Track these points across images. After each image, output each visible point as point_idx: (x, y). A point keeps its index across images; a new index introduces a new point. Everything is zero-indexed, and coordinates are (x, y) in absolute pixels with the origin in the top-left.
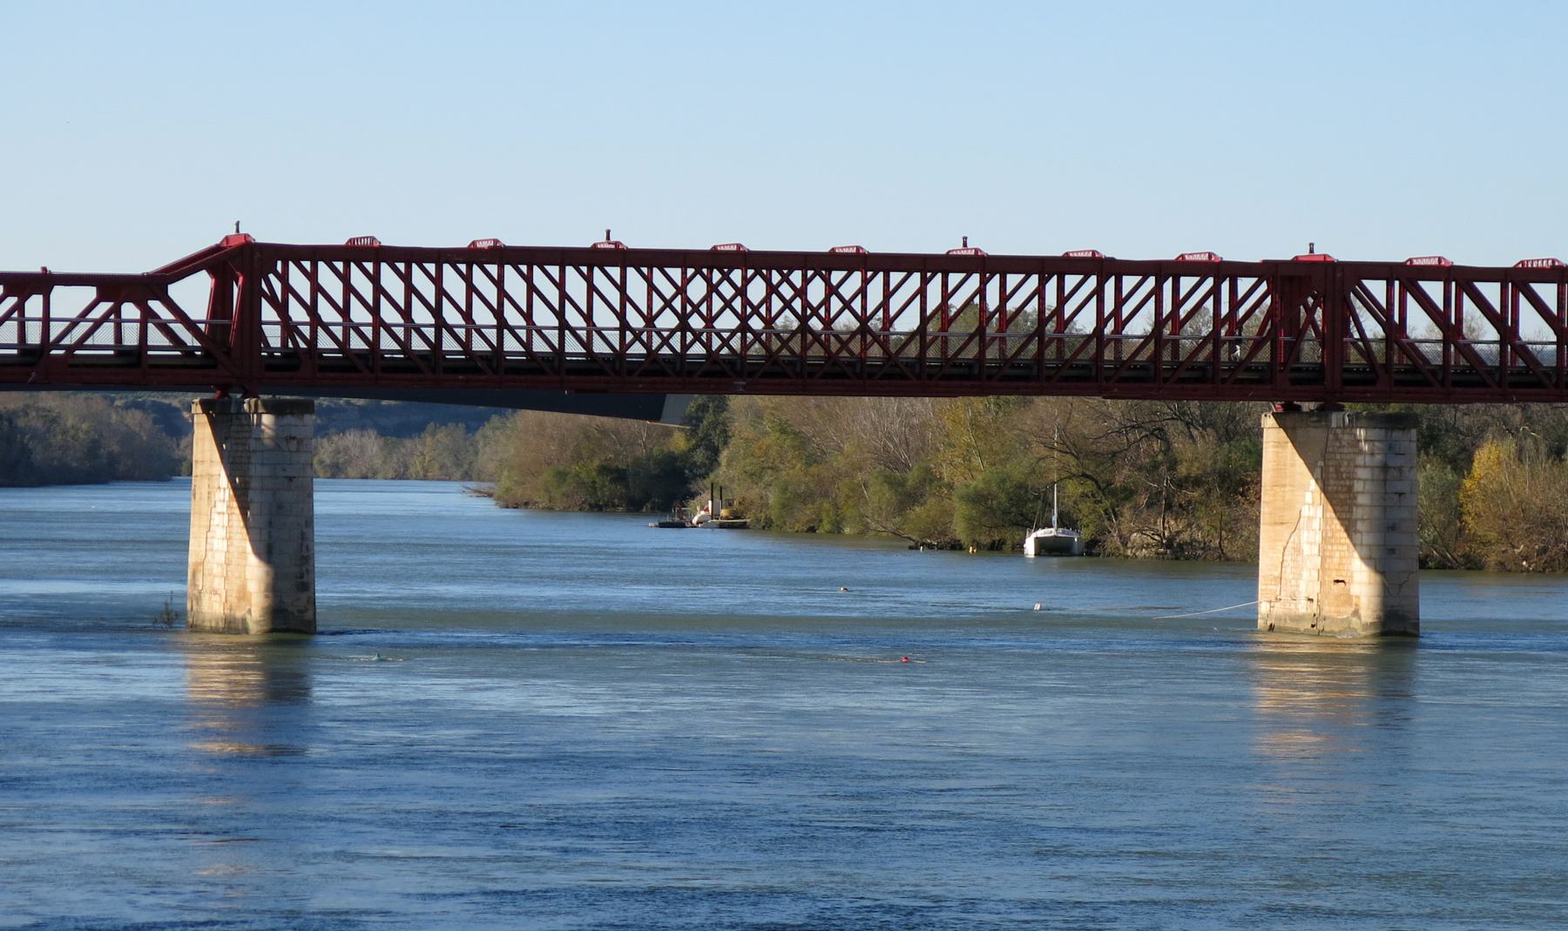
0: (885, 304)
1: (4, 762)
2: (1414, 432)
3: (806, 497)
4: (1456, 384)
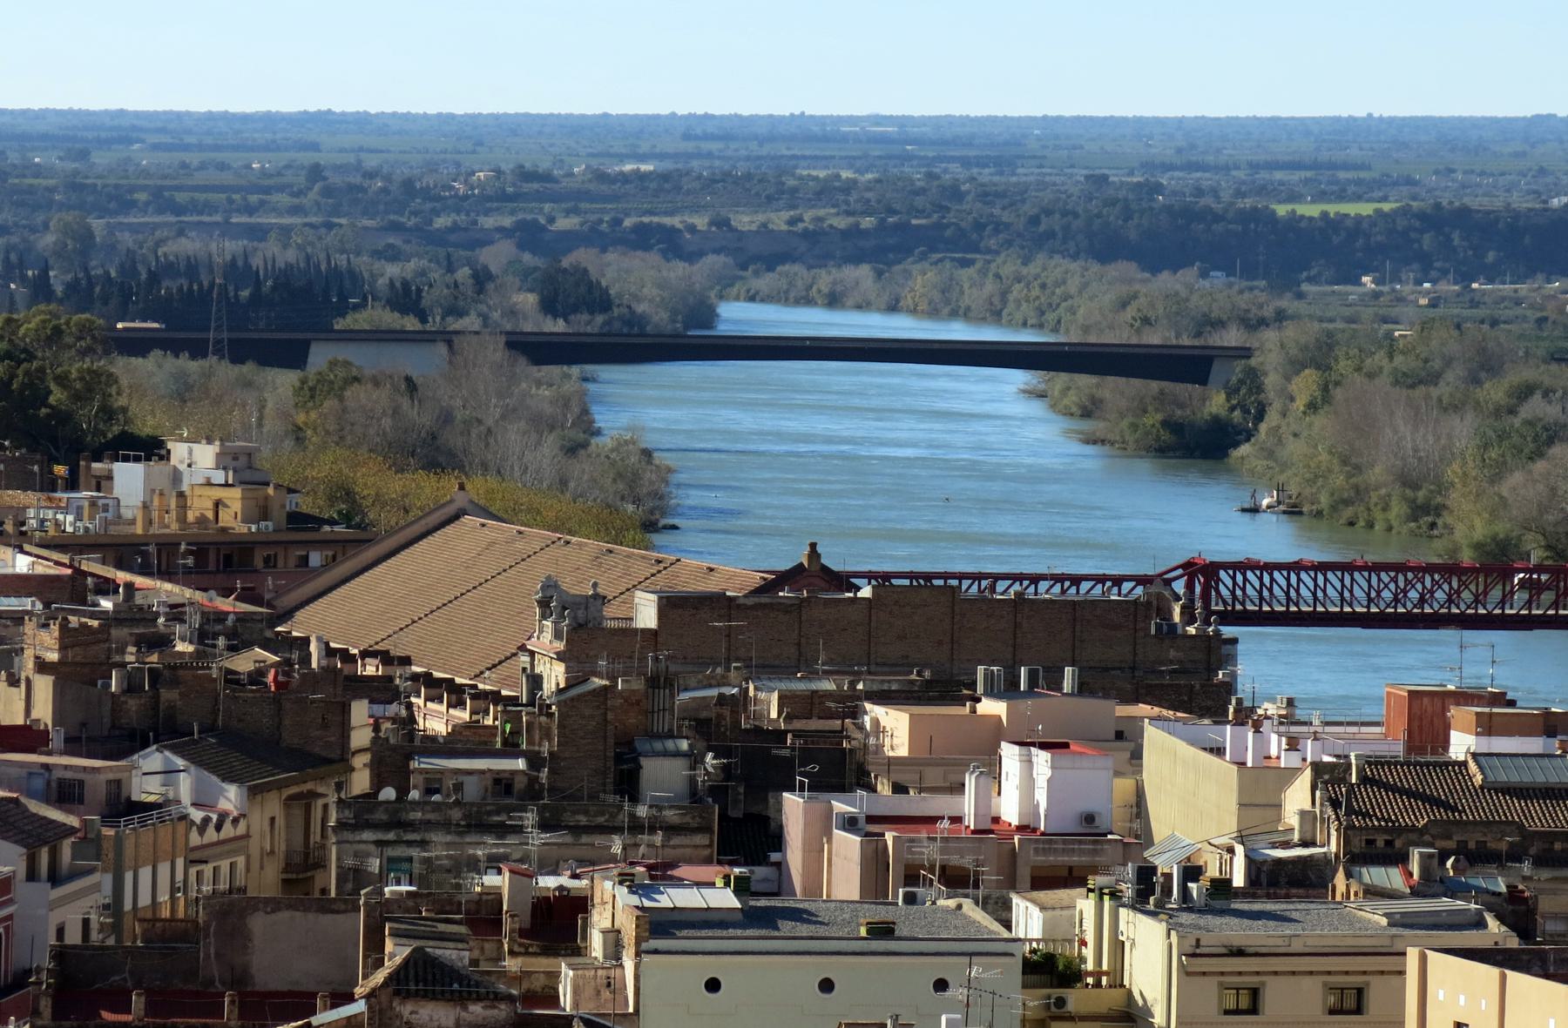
0: (1558, 582)
1: (1158, 1018)
3: (1347, 502)
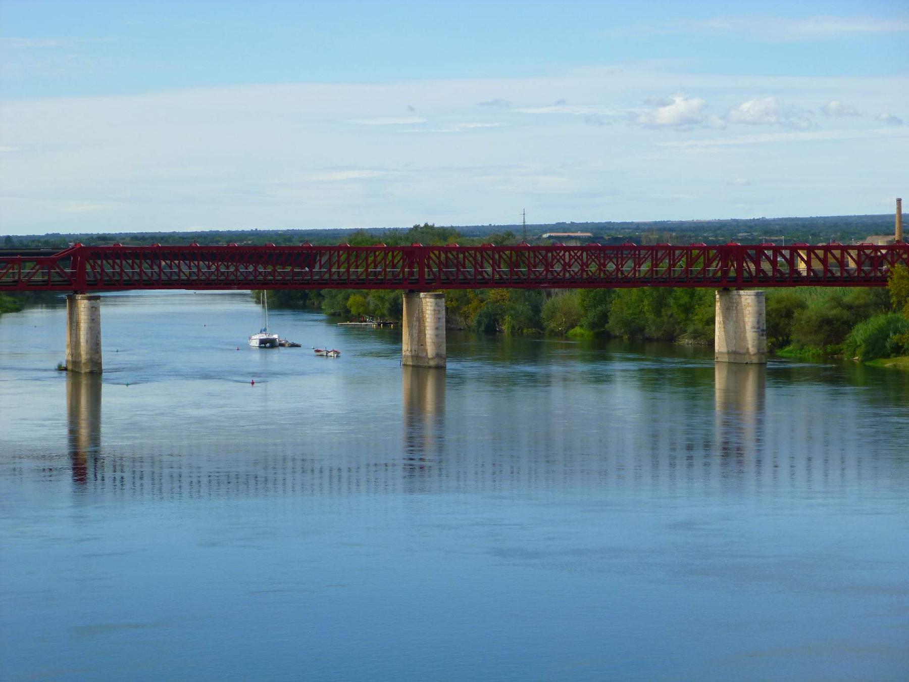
2: (444, 299)
4: (461, 283)
